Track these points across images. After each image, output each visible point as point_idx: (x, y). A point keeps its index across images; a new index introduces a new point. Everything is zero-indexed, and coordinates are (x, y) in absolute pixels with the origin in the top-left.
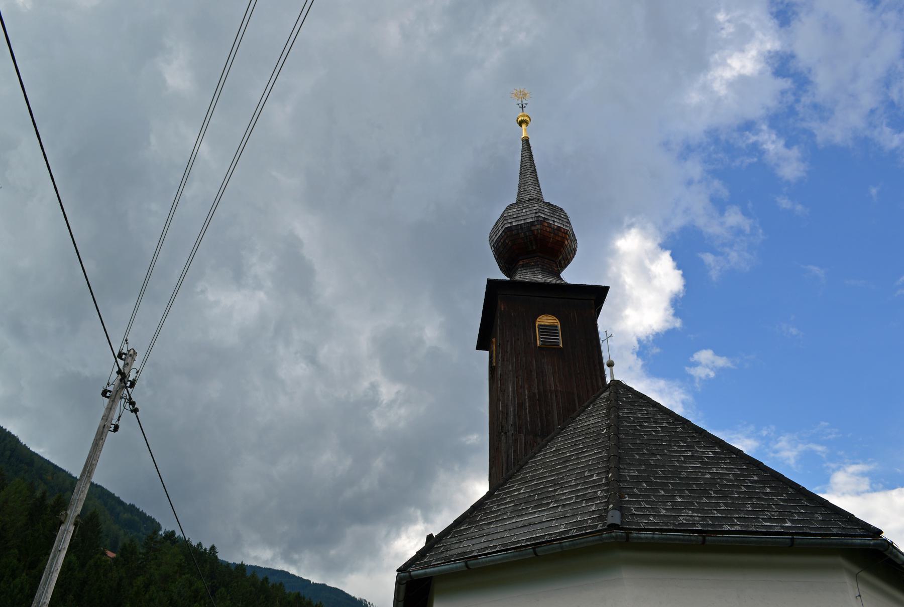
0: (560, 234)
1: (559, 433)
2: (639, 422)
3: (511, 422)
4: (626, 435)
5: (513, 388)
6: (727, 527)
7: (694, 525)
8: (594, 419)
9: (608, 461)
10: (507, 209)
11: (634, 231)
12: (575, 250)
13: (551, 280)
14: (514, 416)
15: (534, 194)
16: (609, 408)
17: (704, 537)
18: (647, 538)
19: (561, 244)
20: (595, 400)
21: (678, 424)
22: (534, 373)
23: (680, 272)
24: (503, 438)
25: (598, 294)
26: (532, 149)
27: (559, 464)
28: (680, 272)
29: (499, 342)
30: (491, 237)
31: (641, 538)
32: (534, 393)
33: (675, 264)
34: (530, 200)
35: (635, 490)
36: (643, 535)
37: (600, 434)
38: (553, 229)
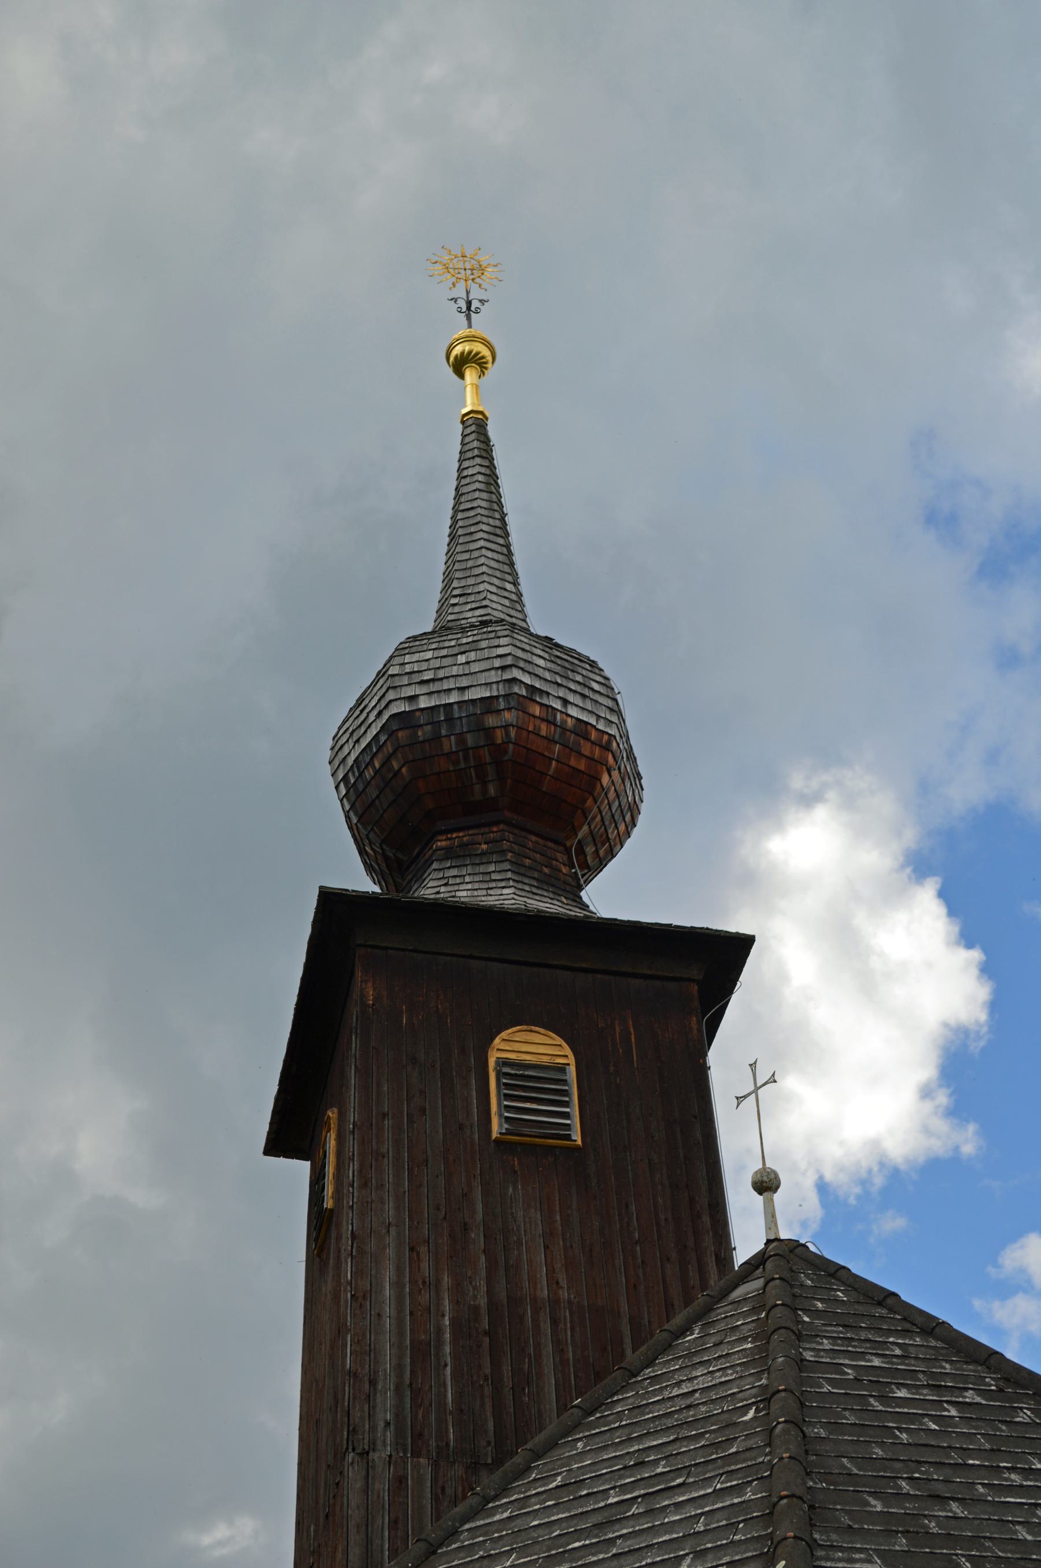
0: (586, 748)
1: (576, 1426)
2: (879, 1383)
3: (385, 1413)
4: (834, 1426)
5: (398, 1285)
8: (709, 1372)
9: (769, 1517)
10: (401, 650)
11: (821, 813)
12: (634, 810)
14: (398, 1389)
15: (497, 609)
16: (763, 1335)
19: (587, 782)
20: (709, 1309)
21: (1019, 1398)
22: (477, 1237)
23: (976, 955)
24: (354, 1475)
25: (720, 958)
26: (498, 454)
27: (578, 1534)
28: (976, 955)
29: (352, 1117)
32: (476, 1309)
33: (956, 929)
34: (484, 624)
38: (564, 729)
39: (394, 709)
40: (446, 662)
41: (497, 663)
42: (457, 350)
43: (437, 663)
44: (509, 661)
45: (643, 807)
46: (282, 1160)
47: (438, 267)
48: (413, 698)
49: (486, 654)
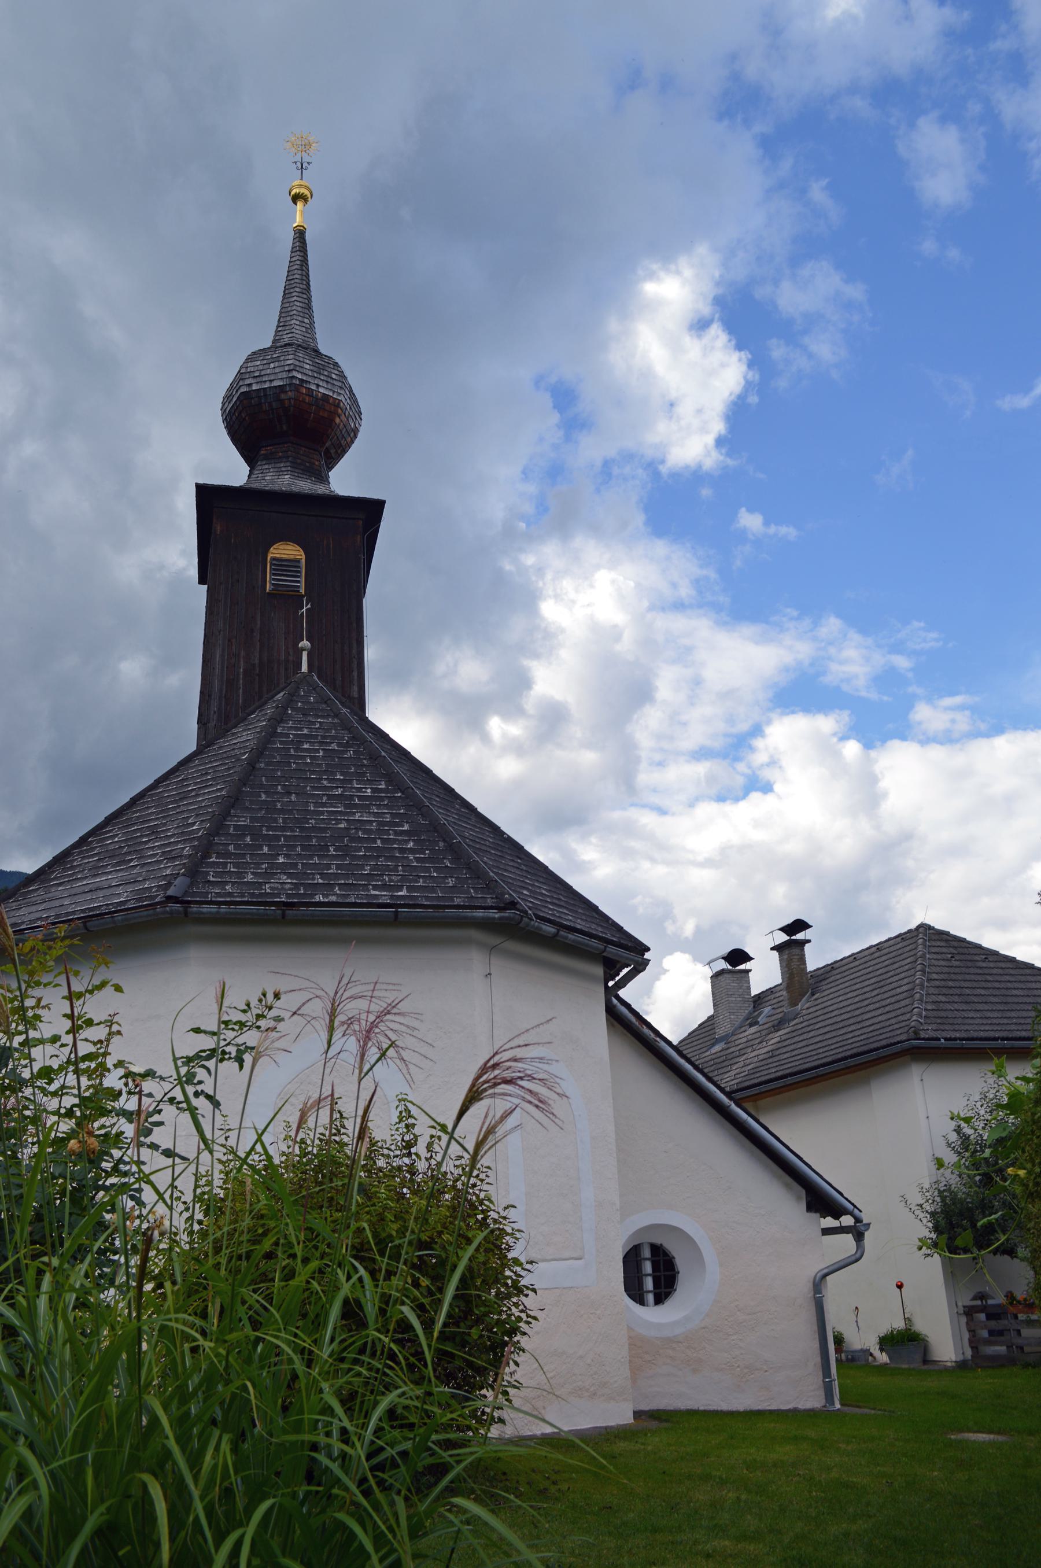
5: (222, 656)
6: (319, 898)
7: (278, 895)
10: (248, 360)
12: (355, 432)
13: (304, 486)
17: (284, 911)
18: (210, 913)
27: (171, 802)
30: (223, 404)
31: (203, 913)
32: (254, 665)
35: (231, 848)
36: (205, 909)
37: (239, 760)
39: (242, 390)
40: (266, 367)
41: (287, 368)
42: (293, 193)
43: (261, 367)
44: (292, 367)
45: (361, 429)
46: (376, 497)
47: (289, 144)
48: (250, 385)
49: (282, 363)
